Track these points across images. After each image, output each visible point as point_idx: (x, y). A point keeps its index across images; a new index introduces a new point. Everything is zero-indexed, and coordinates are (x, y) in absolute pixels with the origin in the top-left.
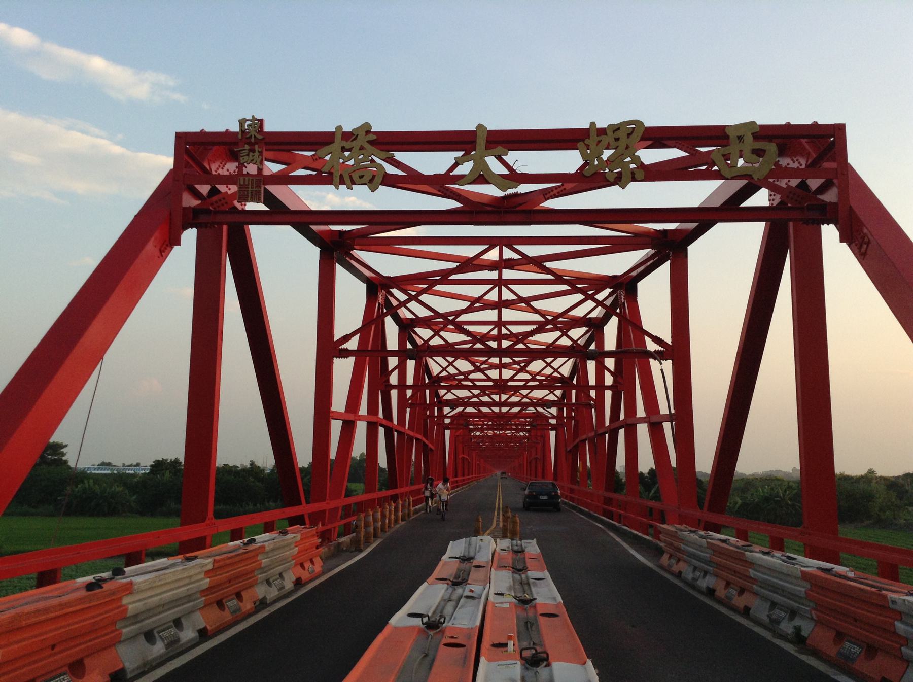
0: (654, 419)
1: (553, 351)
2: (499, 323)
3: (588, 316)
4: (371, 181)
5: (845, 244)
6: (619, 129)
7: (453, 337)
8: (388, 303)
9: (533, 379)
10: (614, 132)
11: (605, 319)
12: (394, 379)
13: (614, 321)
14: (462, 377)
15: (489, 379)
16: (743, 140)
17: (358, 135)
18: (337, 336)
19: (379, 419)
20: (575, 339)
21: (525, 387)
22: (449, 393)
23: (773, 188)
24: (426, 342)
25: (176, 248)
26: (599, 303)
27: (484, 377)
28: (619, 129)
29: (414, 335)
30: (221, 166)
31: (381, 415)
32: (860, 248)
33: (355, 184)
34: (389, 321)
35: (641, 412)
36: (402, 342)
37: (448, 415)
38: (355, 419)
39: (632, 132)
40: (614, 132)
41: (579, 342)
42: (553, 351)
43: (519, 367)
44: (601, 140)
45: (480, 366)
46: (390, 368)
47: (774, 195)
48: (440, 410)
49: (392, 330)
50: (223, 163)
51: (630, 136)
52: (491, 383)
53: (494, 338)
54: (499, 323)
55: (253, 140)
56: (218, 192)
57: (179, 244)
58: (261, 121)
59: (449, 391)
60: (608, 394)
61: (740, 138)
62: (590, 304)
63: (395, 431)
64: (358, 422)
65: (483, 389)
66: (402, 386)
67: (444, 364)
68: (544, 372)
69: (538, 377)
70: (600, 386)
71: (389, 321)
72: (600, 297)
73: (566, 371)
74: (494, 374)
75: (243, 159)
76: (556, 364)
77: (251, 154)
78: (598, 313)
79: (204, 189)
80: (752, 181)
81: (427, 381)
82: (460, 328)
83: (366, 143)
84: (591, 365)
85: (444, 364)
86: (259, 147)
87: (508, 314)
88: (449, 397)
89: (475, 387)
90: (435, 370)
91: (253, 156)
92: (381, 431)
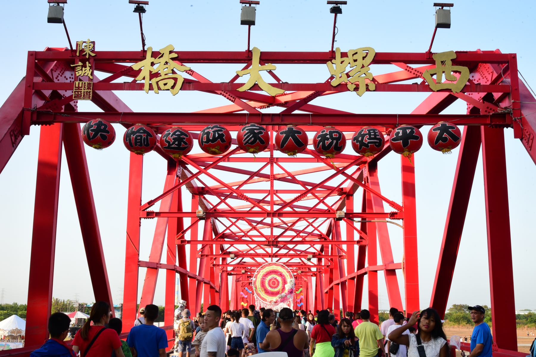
0: (390, 267)
1: (314, 213)
2: (272, 192)
3: (341, 187)
4: (173, 87)
5: (518, 140)
6: (356, 53)
7: (235, 204)
8: (184, 175)
9: (298, 236)
10: (353, 55)
11: (354, 189)
12: (188, 236)
13: (360, 191)
14: (243, 234)
15: (262, 235)
16: (445, 65)
17: (163, 54)
18: (144, 201)
19: (175, 267)
20: (330, 205)
21: (291, 242)
22: (312, 248)
23: (468, 100)
24: (215, 207)
25: (26, 136)
26: (349, 177)
27: (259, 234)
28: (356, 53)
29: (203, 200)
30: (61, 74)
31: (177, 264)
32: (528, 142)
33: (161, 90)
34: (184, 188)
35: (380, 262)
36: (194, 206)
37: (230, 264)
38: (157, 267)
39: (366, 56)
40: (353, 55)
41: (333, 207)
42: (314, 213)
43: (286, 226)
44: (344, 61)
45: (256, 225)
46: (185, 228)
47: (470, 105)
48: (224, 259)
49: (186, 196)
50: (62, 72)
51: (365, 59)
52: (263, 239)
53: (267, 202)
54: (272, 192)
55: (87, 57)
56: (60, 96)
57: (28, 134)
58: (94, 43)
59: (232, 245)
60: (356, 248)
61: (443, 63)
62: (341, 178)
63: (188, 277)
64: (160, 269)
65: (259, 243)
66: (194, 242)
67: (228, 224)
68: (306, 230)
69: (301, 234)
70: (350, 242)
71: (184, 188)
72: (349, 171)
73: (324, 229)
74: (267, 231)
75: (78, 73)
76: (316, 224)
77: (84, 69)
78: (348, 185)
79: (47, 93)
80: (452, 93)
81: (214, 237)
82: (241, 196)
83: (171, 60)
84: (343, 225)
85: (228, 224)
86: (89, 63)
87: (278, 185)
88: (232, 249)
89: (253, 242)
90: (221, 229)
91: (85, 70)
92: (178, 276)
